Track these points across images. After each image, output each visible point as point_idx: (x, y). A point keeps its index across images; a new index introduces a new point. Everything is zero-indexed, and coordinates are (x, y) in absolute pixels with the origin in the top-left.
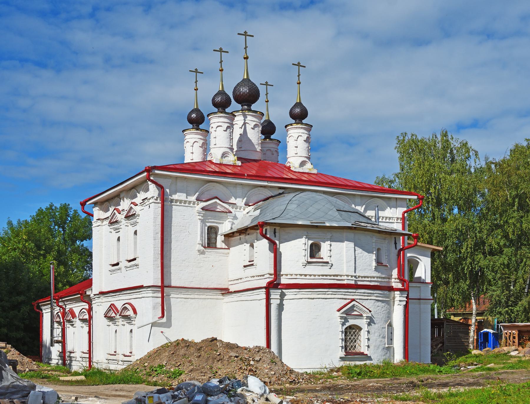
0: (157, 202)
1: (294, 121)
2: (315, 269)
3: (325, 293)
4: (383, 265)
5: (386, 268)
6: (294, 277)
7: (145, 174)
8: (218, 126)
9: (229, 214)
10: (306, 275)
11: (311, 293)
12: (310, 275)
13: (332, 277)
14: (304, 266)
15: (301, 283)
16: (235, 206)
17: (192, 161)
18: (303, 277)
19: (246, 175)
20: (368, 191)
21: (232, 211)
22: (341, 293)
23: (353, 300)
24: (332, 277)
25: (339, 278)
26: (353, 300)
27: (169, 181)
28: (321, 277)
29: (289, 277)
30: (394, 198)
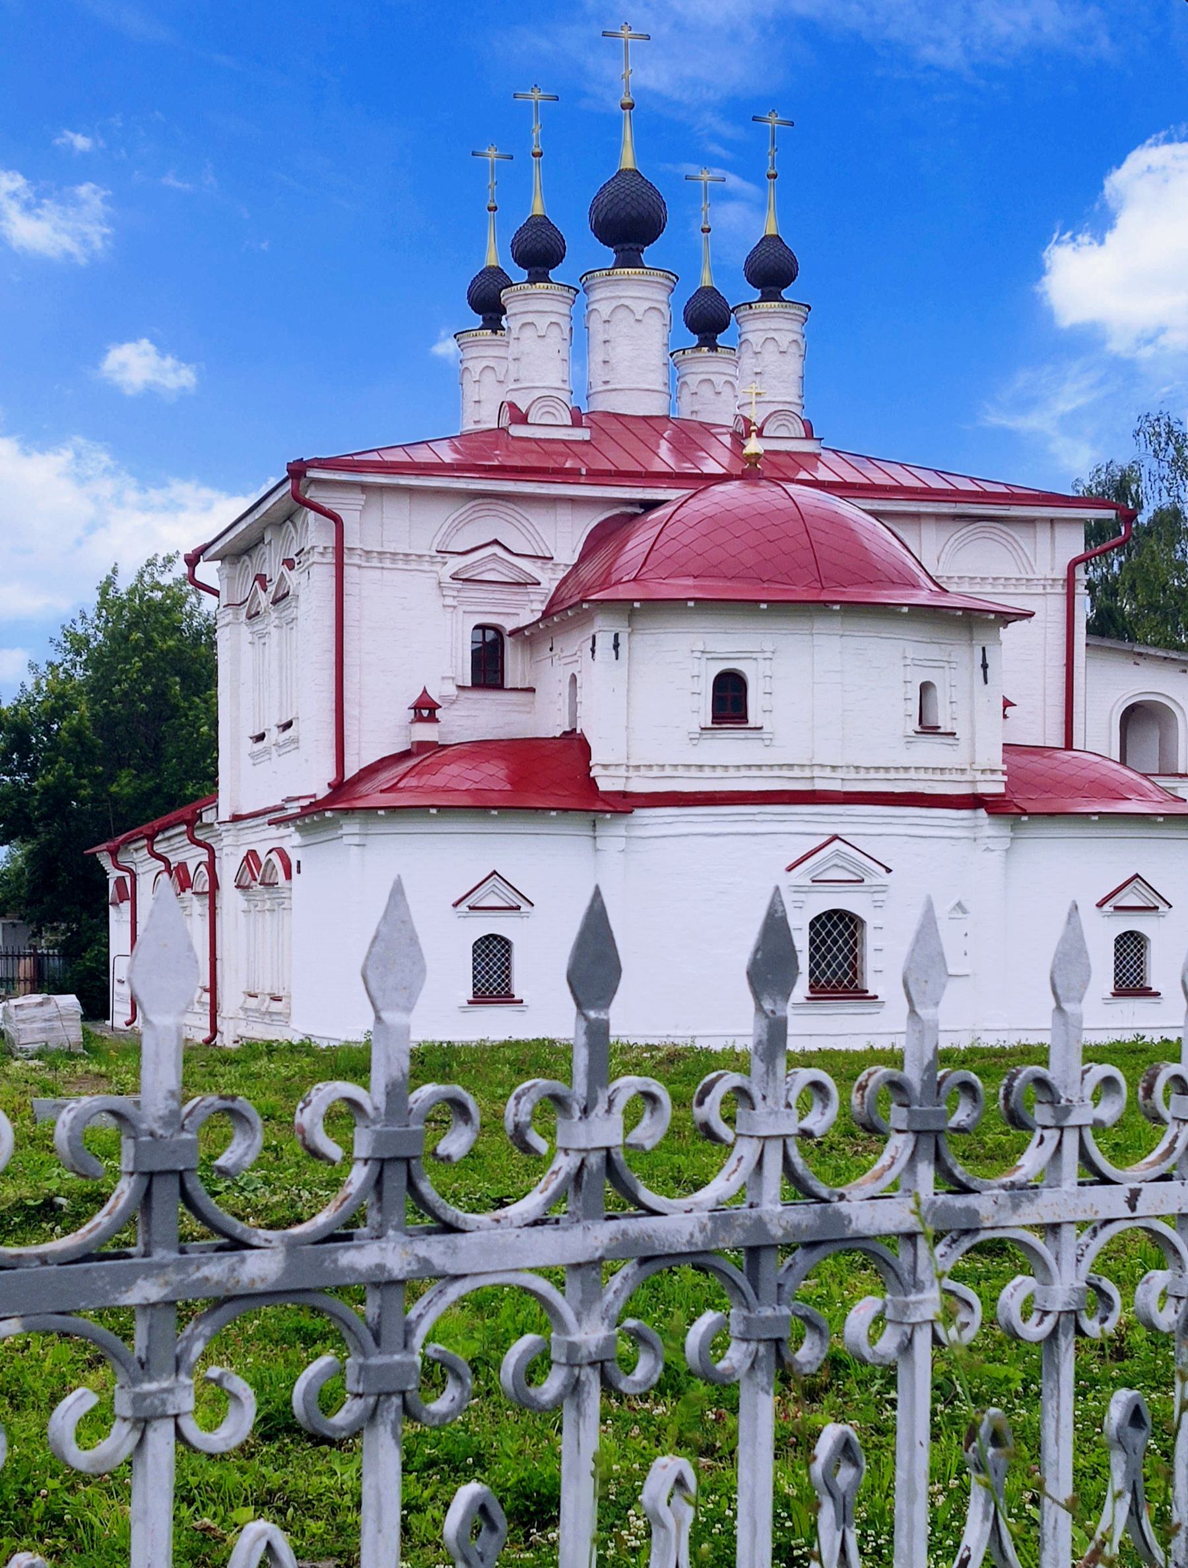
0: (325, 561)
1: (758, 293)
2: (931, 752)
3: (751, 818)
4: (941, 731)
5: (949, 740)
6: (668, 772)
7: (288, 486)
8: (524, 325)
9: (531, 589)
10: (700, 767)
11: (776, 817)
12: (701, 767)
13: (776, 773)
14: (695, 742)
15: (928, 791)
16: (550, 565)
17: (694, 418)
18: (694, 773)
19: (584, 472)
20: (955, 502)
21: (540, 580)
22: (801, 818)
23: (836, 837)
24: (776, 773)
25: (796, 773)
26: (836, 837)
27: (359, 498)
28: (744, 772)
29: (656, 772)
30: (1043, 520)
